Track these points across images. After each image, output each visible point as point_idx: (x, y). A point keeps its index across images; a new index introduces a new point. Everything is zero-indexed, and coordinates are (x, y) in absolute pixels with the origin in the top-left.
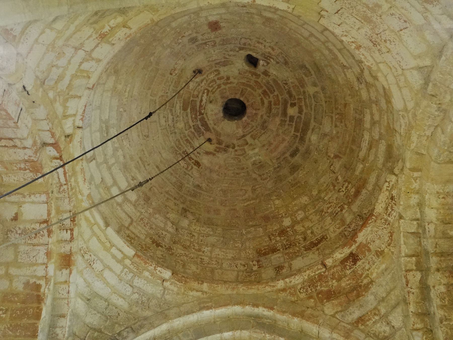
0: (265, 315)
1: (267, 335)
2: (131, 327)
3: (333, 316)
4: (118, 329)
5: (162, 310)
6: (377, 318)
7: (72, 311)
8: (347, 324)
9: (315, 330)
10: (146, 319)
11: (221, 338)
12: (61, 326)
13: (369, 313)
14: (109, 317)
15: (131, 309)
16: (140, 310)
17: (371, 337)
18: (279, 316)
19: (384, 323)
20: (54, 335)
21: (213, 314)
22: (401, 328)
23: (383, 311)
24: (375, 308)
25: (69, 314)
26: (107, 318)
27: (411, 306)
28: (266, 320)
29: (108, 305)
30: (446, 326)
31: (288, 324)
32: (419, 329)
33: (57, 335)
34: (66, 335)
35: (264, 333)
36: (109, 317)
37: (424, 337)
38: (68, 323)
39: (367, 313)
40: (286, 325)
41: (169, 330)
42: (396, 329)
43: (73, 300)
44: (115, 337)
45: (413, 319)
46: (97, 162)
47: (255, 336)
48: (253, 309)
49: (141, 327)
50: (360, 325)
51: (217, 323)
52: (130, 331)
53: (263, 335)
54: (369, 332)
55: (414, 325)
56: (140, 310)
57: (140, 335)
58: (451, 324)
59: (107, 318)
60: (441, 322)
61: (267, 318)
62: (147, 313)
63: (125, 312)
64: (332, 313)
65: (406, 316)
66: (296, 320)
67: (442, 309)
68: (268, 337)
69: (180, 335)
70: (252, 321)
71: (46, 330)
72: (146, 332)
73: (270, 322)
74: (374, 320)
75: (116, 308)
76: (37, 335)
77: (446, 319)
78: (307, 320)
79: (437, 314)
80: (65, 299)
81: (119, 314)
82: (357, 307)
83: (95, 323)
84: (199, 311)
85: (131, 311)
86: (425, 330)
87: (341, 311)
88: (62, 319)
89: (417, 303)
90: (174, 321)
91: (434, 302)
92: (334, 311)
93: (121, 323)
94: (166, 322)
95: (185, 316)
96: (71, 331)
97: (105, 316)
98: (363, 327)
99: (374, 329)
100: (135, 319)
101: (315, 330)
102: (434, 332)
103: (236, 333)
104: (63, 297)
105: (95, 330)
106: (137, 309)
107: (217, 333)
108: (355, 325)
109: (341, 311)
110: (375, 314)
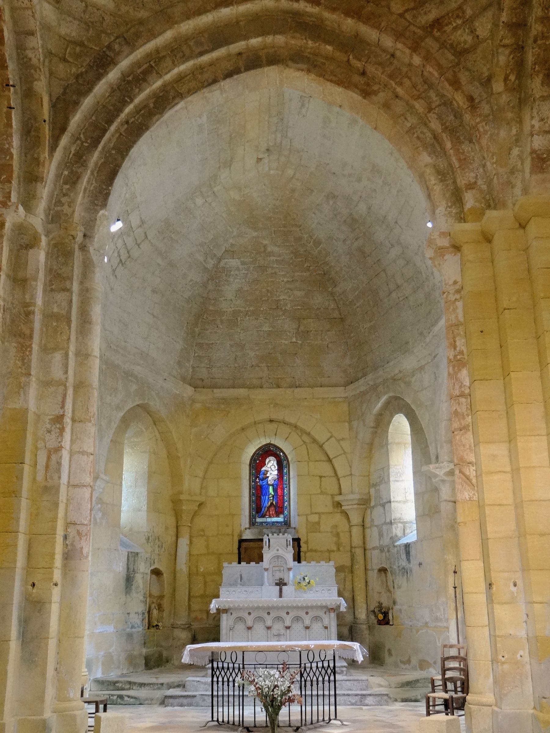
0: (307, 12)
1: (310, 42)
2: (123, 37)
3: (401, 15)
4: (106, 40)
5: (162, 8)
6: (459, 22)
7: (40, 23)
8: (419, 28)
9: (374, 36)
10: (141, 22)
11: (247, 45)
12: (31, 47)
13: (450, 15)
14: (90, 24)
15: (119, 10)
16: (131, 11)
17: (446, 48)
18: (326, 15)
19: (467, 30)
20: (25, 60)
21: (234, 11)
22: (487, 39)
23: (469, 12)
24: (460, 8)
25: (38, 30)
26: (89, 26)
27: (504, 14)
28: (308, 18)
29: (86, 6)
30: (540, 47)
31: (339, 26)
32: (508, 46)
33: (30, 59)
34: (42, 59)
35: (306, 39)
36: (90, 24)
37: (512, 56)
38: (40, 42)
39: (448, 14)
40: (336, 25)
41: (175, 38)
42: (480, 40)
43: (38, 7)
44: (104, 52)
45: (502, 33)
46: (333, 551)
47: (293, 42)
48: (291, 3)
49: (137, 35)
50: (436, 30)
51: (241, 23)
52: (123, 43)
53: (305, 41)
54: (445, 41)
55: (501, 41)
56: (131, 11)
57: (138, 49)
58: (547, 43)
59: (88, 25)
60: (535, 41)
61: (310, 15)
62: (143, 14)
63: (111, 15)
64: (401, 11)
65: (496, 25)
66: (349, 21)
67: (542, 22)
68: (311, 45)
69: (192, 43)
70: (289, 20)
71: (14, 55)
72: (145, 43)
73: (314, 21)
74: (454, 25)
75: (98, 10)
76: (7, 66)
77: (543, 37)
78: (364, 23)
79: (533, 29)
80: (27, 8)
81: (103, 18)
82: (435, 4)
83: (74, 34)
84: (215, 9)
85: (119, 13)
86: (515, 46)
87: (413, 9)
88: (31, 38)
89: (514, 9)
90: (182, 25)
91: (535, 10)
92: (404, 9)
93: (109, 31)
94: (170, 28)
95: (197, 18)
96: (46, 50)
97: (86, 23)
98: (439, 34)
99: (452, 37)
100: (127, 24)
101: (374, 36)
102: (525, 50)
103: (267, 38)
104: (24, 6)
105: (75, 43)
106: (127, 8)
107: (240, 40)
108: (429, 29)
109: (413, 9)
110: (458, 17)
